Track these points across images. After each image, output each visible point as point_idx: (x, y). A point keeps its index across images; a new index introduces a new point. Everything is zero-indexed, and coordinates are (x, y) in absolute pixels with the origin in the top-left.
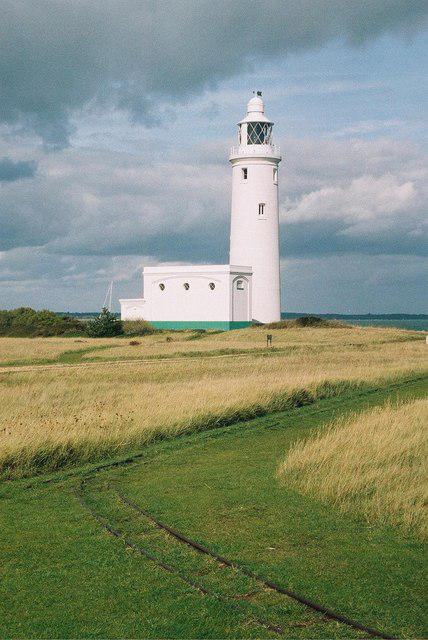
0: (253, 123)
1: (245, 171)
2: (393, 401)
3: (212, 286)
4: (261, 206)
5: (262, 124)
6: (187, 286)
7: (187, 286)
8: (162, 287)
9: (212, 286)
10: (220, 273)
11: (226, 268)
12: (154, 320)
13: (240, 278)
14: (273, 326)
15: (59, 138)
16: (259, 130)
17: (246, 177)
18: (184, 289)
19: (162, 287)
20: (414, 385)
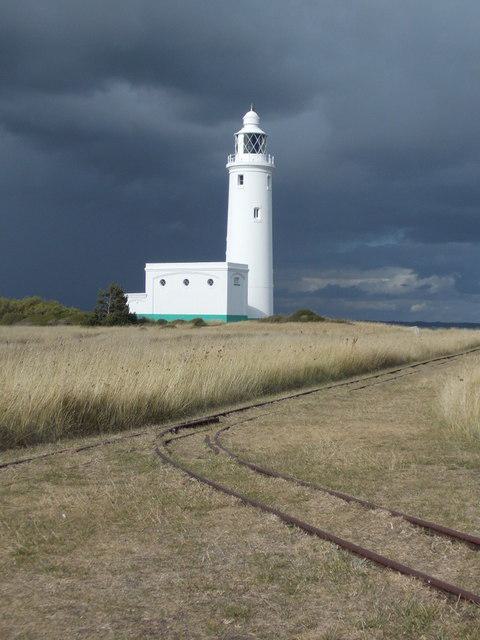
0: (250, 134)
1: (241, 177)
2: (139, 409)
3: (211, 282)
4: (256, 211)
5: (258, 135)
6: (186, 282)
7: (186, 282)
8: (163, 282)
9: (211, 282)
10: (218, 270)
11: (223, 266)
12: (209, 314)
13: (238, 276)
14: (264, 320)
15: (245, 152)
16: (254, 140)
17: (242, 183)
18: (237, 287)
19: (163, 282)
20: (473, 348)
